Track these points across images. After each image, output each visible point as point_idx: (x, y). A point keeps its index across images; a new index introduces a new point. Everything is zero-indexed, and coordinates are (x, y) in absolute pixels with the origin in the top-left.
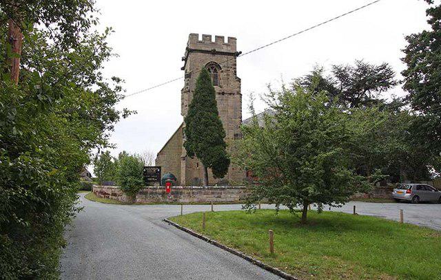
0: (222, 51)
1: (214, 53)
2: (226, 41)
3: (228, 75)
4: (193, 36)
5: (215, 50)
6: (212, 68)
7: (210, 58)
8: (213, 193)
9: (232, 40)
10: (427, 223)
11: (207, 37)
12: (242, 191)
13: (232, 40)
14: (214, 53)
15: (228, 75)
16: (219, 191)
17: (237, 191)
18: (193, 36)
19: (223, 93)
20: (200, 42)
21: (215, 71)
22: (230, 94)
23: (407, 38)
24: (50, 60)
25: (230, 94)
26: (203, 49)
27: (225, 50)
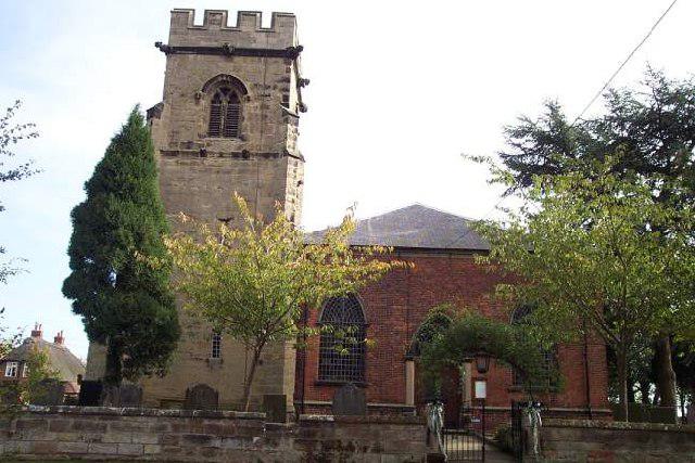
0: (254, 46)
1: (226, 52)
2: (266, 23)
3: (264, 107)
4: (180, 17)
5: (226, 47)
6: (225, 91)
7: (223, 67)
8: (77, 427)
9: (284, 20)
10: (81, 444)
11: (213, 16)
12: (167, 423)
13: (284, 20)
14: (226, 52)
15: (264, 107)
16: (96, 421)
17: (152, 422)
18: (180, 17)
19: (245, 155)
20: (198, 28)
21: (234, 96)
22: (266, 156)
23: (300, 48)
24: (193, 38)
25: (266, 156)
26: (203, 44)
27: (261, 43)
